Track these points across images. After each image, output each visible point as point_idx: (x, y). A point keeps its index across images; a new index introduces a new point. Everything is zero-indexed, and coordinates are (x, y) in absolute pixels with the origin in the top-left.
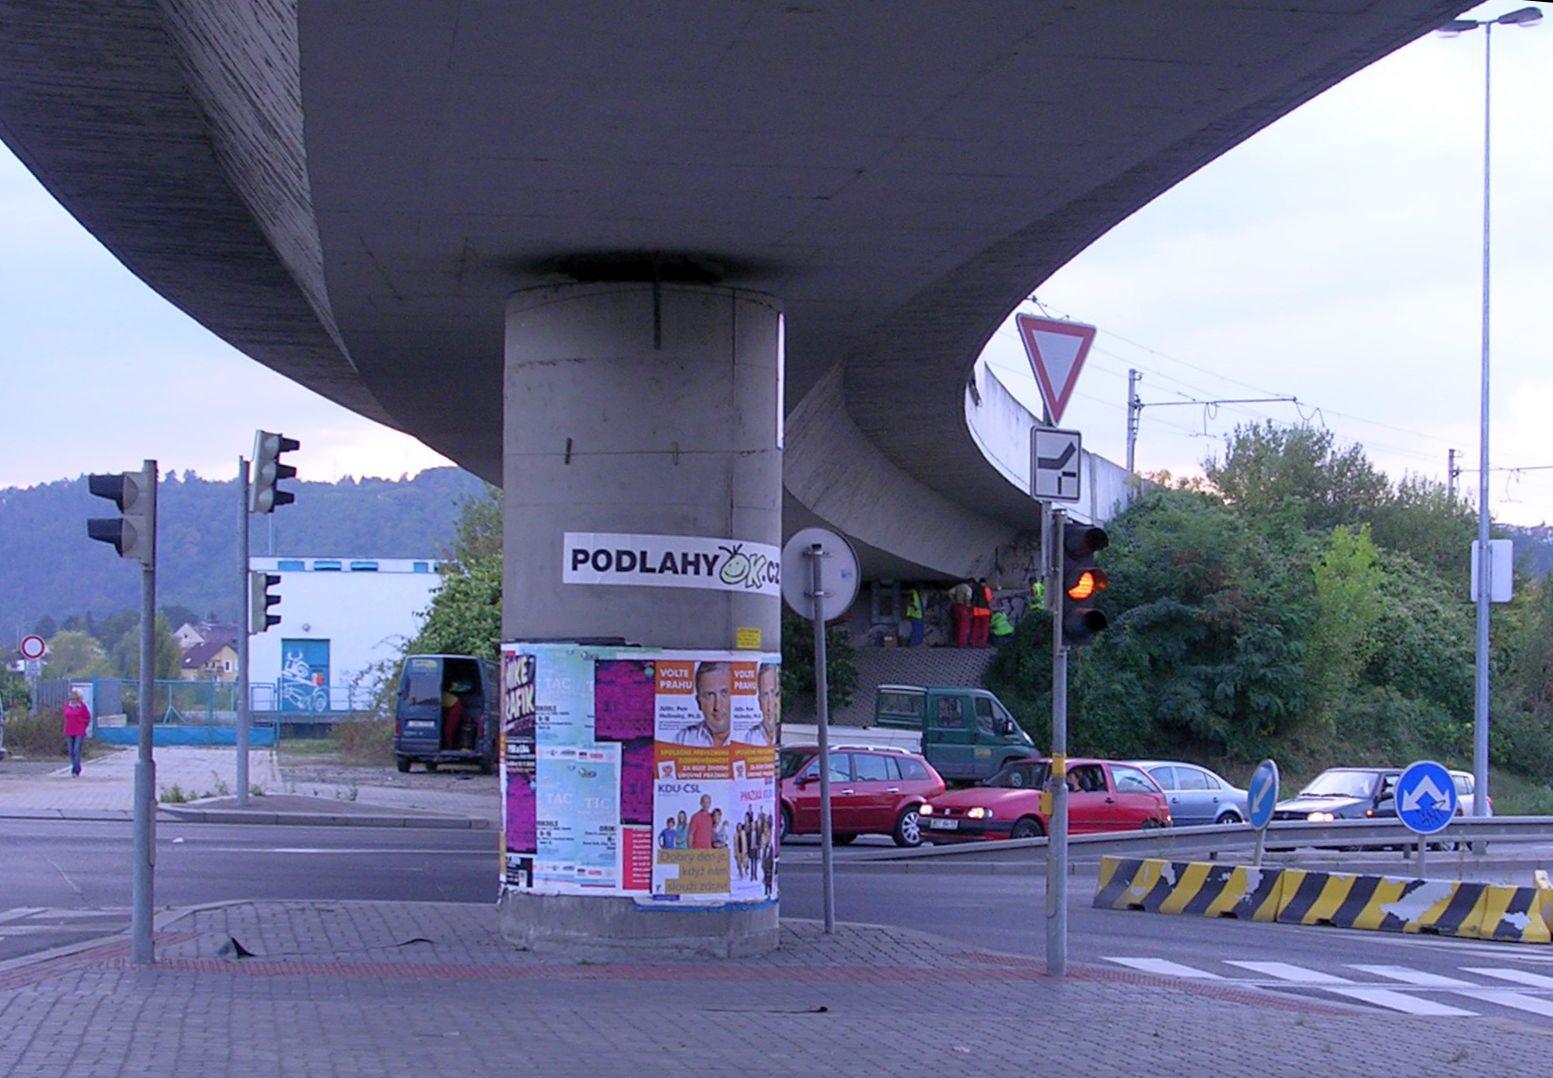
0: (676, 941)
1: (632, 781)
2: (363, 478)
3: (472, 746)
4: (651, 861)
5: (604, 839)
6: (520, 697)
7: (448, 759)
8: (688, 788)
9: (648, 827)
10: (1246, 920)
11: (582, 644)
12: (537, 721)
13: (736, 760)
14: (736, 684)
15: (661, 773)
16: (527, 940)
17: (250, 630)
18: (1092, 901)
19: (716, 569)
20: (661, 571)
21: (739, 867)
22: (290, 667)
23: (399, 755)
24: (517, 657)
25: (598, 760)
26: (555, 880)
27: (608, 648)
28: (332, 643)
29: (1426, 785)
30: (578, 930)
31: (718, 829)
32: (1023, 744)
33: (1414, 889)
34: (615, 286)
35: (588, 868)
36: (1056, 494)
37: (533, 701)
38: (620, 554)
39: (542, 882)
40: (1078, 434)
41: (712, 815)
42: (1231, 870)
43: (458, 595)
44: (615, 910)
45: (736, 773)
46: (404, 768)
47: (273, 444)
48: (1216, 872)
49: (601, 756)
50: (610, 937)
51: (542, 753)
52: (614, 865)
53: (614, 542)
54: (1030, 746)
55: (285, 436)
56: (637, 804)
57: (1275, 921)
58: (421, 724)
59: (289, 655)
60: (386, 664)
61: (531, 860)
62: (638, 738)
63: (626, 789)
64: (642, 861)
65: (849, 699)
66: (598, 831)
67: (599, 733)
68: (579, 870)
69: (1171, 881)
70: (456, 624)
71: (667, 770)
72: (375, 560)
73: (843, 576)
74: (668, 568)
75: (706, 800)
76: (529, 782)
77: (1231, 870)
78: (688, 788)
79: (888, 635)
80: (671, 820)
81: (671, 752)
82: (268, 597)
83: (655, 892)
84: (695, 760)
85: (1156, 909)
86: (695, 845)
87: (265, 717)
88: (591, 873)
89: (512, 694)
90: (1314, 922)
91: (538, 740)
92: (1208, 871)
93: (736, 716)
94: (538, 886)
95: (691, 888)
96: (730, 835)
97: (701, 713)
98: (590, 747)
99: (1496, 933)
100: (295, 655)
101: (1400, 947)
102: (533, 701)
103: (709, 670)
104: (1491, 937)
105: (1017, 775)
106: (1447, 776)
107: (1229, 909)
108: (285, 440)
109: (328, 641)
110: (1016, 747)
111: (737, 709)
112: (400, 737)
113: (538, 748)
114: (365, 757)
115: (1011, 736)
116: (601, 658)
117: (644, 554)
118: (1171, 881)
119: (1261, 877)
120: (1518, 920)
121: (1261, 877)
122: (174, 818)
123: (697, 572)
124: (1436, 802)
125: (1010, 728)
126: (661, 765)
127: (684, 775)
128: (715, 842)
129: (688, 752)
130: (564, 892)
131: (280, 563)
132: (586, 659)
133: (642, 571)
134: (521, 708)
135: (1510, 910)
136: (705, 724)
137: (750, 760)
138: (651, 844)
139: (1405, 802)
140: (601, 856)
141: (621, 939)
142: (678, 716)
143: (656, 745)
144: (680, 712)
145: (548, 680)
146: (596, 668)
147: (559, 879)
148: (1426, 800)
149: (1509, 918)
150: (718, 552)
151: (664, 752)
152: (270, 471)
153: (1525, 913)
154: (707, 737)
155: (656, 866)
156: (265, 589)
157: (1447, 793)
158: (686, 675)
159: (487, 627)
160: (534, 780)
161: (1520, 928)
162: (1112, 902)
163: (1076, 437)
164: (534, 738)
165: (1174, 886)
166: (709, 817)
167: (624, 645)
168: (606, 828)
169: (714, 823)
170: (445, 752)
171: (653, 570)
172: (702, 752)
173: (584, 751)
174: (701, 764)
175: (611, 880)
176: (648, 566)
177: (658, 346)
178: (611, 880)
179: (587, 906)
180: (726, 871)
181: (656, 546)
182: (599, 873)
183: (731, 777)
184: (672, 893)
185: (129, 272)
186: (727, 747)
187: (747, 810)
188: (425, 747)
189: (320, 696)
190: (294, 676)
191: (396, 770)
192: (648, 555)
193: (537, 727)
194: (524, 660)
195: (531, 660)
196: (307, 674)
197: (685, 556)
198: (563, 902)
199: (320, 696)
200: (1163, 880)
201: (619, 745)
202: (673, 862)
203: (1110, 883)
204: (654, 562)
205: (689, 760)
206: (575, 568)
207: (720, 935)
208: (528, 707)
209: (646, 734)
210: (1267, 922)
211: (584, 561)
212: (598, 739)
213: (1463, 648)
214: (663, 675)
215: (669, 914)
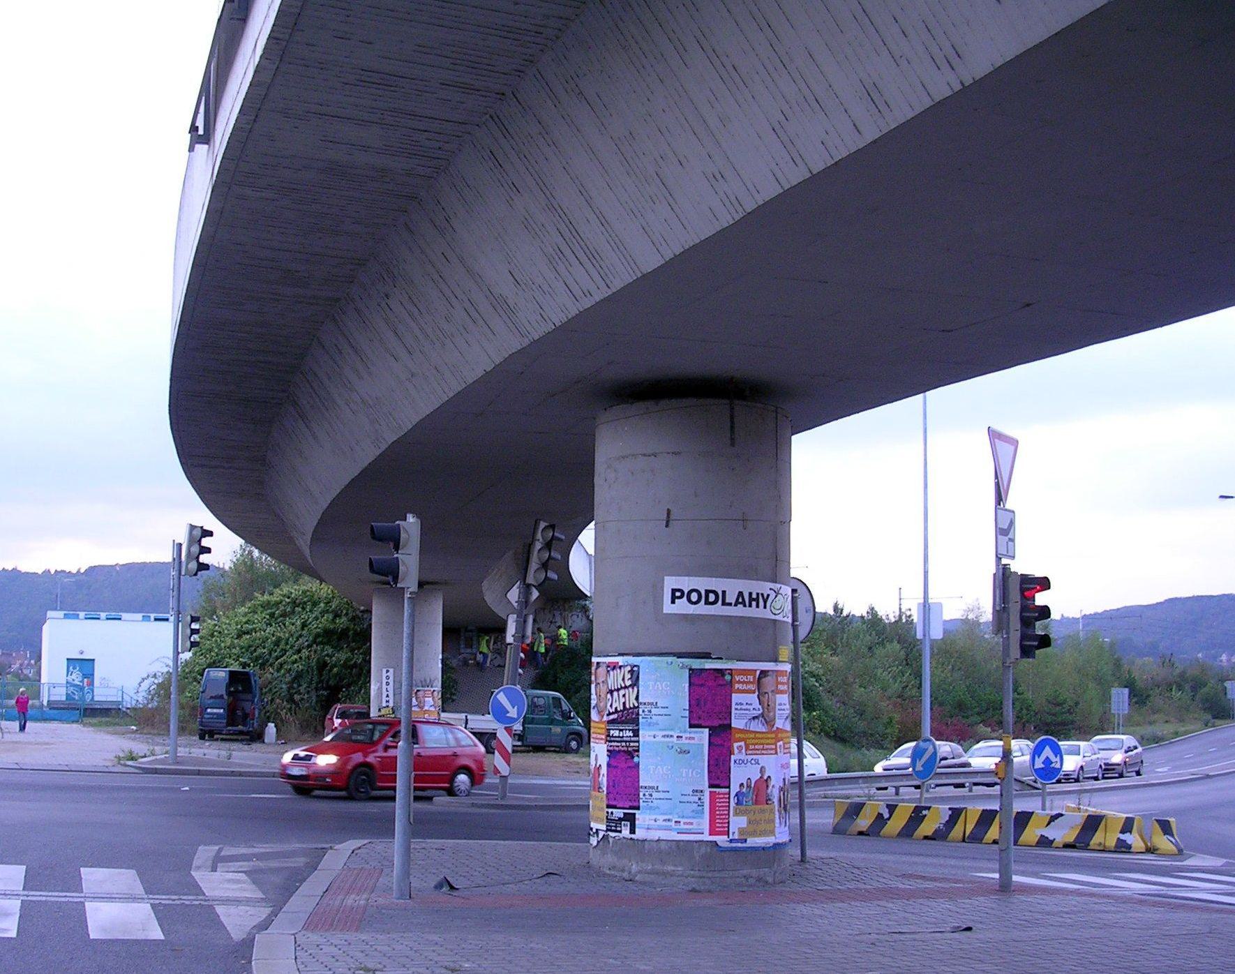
0: (745, 872)
1: (716, 757)
2: (56, 571)
3: (244, 725)
4: (729, 814)
5: (696, 799)
6: (624, 696)
7: (231, 732)
8: (753, 762)
9: (728, 790)
10: (943, 840)
11: (678, 658)
12: (641, 712)
13: (779, 741)
14: (780, 686)
15: (736, 751)
16: (630, 873)
17: (180, 650)
18: (831, 828)
19: (768, 604)
20: (736, 605)
21: (780, 818)
22: (71, 675)
23: (201, 730)
24: (620, 667)
25: (692, 742)
26: (656, 829)
27: (699, 660)
28: (96, 661)
29: (1048, 752)
30: (675, 866)
31: (769, 791)
32: (578, 725)
33: (1056, 819)
34: (701, 401)
35: (683, 821)
36: (1006, 553)
37: (637, 698)
38: (707, 592)
39: (645, 831)
40: (1013, 512)
41: (766, 780)
42: (929, 808)
43: (215, 633)
44: (703, 850)
45: (778, 750)
46: (202, 737)
47: (197, 533)
48: (918, 810)
49: (693, 738)
50: (699, 870)
51: (643, 737)
52: (703, 818)
53: (702, 584)
54: (582, 727)
55: (205, 528)
56: (719, 773)
57: (964, 841)
58: (215, 711)
59: (71, 668)
60: (157, 674)
61: (635, 814)
62: (720, 725)
63: (711, 762)
64: (722, 815)
65: (454, 697)
66: (691, 793)
67: (692, 722)
68: (676, 822)
69: (886, 816)
70: (216, 650)
71: (740, 748)
72: (120, 614)
73: (807, 612)
74: (740, 603)
75: (763, 770)
76: (633, 757)
77: (929, 808)
78: (753, 762)
79: (471, 659)
80: (742, 785)
81: (742, 736)
82: (192, 630)
83: (731, 837)
84: (757, 741)
85: (877, 834)
86: (756, 803)
87: (57, 704)
88: (684, 823)
89: (615, 694)
90: (991, 842)
91: (641, 727)
92: (912, 809)
93: (779, 710)
94: (640, 834)
95: (754, 834)
96: (775, 793)
97: (760, 707)
98: (685, 732)
99: (1116, 846)
100: (74, 668)
101: (1058, 856)
102: (637, 698)
103: (765, 677)
104: (1113, 849)
105: (575, 742)
106: (1058, 745)
107: (930, 833)
108: (205, 530)
109: (94, 660)
110: (574, 727)
111: (737, 704)
112: (202, 718)
113: (641, 732)
114: (163, 729)
115: (572, 720)
116: (693, 667)
117: (724, 592)
118: (886, 816)
119: (950, 812)
120: (1126, 837)
121: (950, 812)
122: (136, 771)
123: (758, 606)
124: (1052, 763)
125: (572, 715)
126: (736, 745)
127: (750, 752)
128: (768, 801)
129: (752, 736)
130: (663, 838)
131: (65, 614)
132: (682, 668)
133: (706, 604)
134: (624, 703)
135: (1122, 832)
136: (762, 715)
137: (748, 741)
138: (729, 802)
139: (1036, 763)
140: (693, 811)
141: (707, 872)
142: (747, 710)
143: (733, 730)
144: (748, 707)
145: (651, 683)
146: (690, 674)
147: (660, 828)
148: (1047, 761)
149: (1123, 837)
150: (770, 592)
151: (737, 736)
152: (195, 549)
153: (1131, 832)
154: (763, 725)
155: (732, 819)
156: (190, 625)
157: (1058, 757)
158: (752, 680)
159: (236, 652)
160: (638, 756)
161: (1129, 843)
162: (846, 831)
163: (1012, 514)
164: (638, 725)
165: (889, 819)
166: (764, 782)
167: (711, 658)
168: (697, 791)
169: (767, 786)
170: (230, 728)
171: (730, 604)
172: (760, 736)
173: (681, 735)
174: (760, 744)
175: (700, 829)
176: (727, 601)
177: (733, 444)
178: (700, 829)
179: (681, 849)
180: (773, 821)
181: (732, 587)
182: (692, 824)
183: (776, 753)
184: (742, 837)
185: (168, 411)
186: (774, 732)
187: (783, 777)
188: (218, 725)
189: (88, 692)
190: (73, 680)
191: (197, 738)
192: (727, 592)
193: (640, 717)
194: (629, 668)
195: (635, 669)
196: (81, 679)
197: (750, 594)
198: (663, 845)
199: (88, 692)
200: (880, 816)
201: (707, 730)
202: (743, 815)
203: (842, 818)
204: (731, 598)
205: (753, 741)
206: (673, 602)
207: (770, 867)
208: (632, 702)
209: (726, 722)
210: (958, 842)
211: (680, 597)
212: (691, 726)
213: (807, 669)
214: (737, 679)
215: (742, 854)
